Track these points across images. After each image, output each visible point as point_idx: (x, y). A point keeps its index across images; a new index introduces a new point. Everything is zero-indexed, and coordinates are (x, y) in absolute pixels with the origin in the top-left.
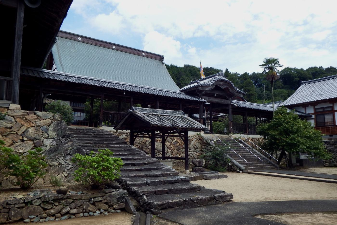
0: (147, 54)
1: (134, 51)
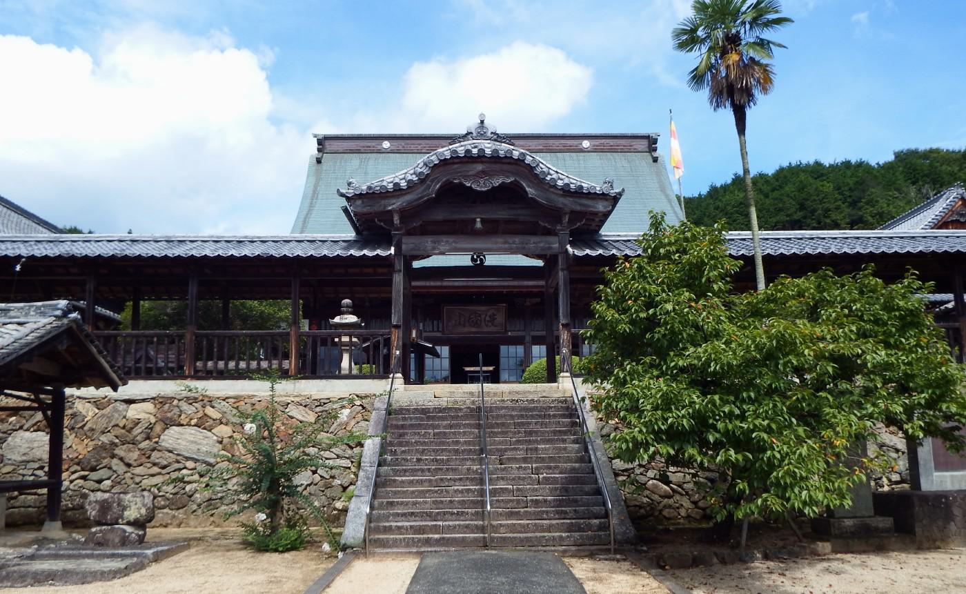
1: (551, 142)
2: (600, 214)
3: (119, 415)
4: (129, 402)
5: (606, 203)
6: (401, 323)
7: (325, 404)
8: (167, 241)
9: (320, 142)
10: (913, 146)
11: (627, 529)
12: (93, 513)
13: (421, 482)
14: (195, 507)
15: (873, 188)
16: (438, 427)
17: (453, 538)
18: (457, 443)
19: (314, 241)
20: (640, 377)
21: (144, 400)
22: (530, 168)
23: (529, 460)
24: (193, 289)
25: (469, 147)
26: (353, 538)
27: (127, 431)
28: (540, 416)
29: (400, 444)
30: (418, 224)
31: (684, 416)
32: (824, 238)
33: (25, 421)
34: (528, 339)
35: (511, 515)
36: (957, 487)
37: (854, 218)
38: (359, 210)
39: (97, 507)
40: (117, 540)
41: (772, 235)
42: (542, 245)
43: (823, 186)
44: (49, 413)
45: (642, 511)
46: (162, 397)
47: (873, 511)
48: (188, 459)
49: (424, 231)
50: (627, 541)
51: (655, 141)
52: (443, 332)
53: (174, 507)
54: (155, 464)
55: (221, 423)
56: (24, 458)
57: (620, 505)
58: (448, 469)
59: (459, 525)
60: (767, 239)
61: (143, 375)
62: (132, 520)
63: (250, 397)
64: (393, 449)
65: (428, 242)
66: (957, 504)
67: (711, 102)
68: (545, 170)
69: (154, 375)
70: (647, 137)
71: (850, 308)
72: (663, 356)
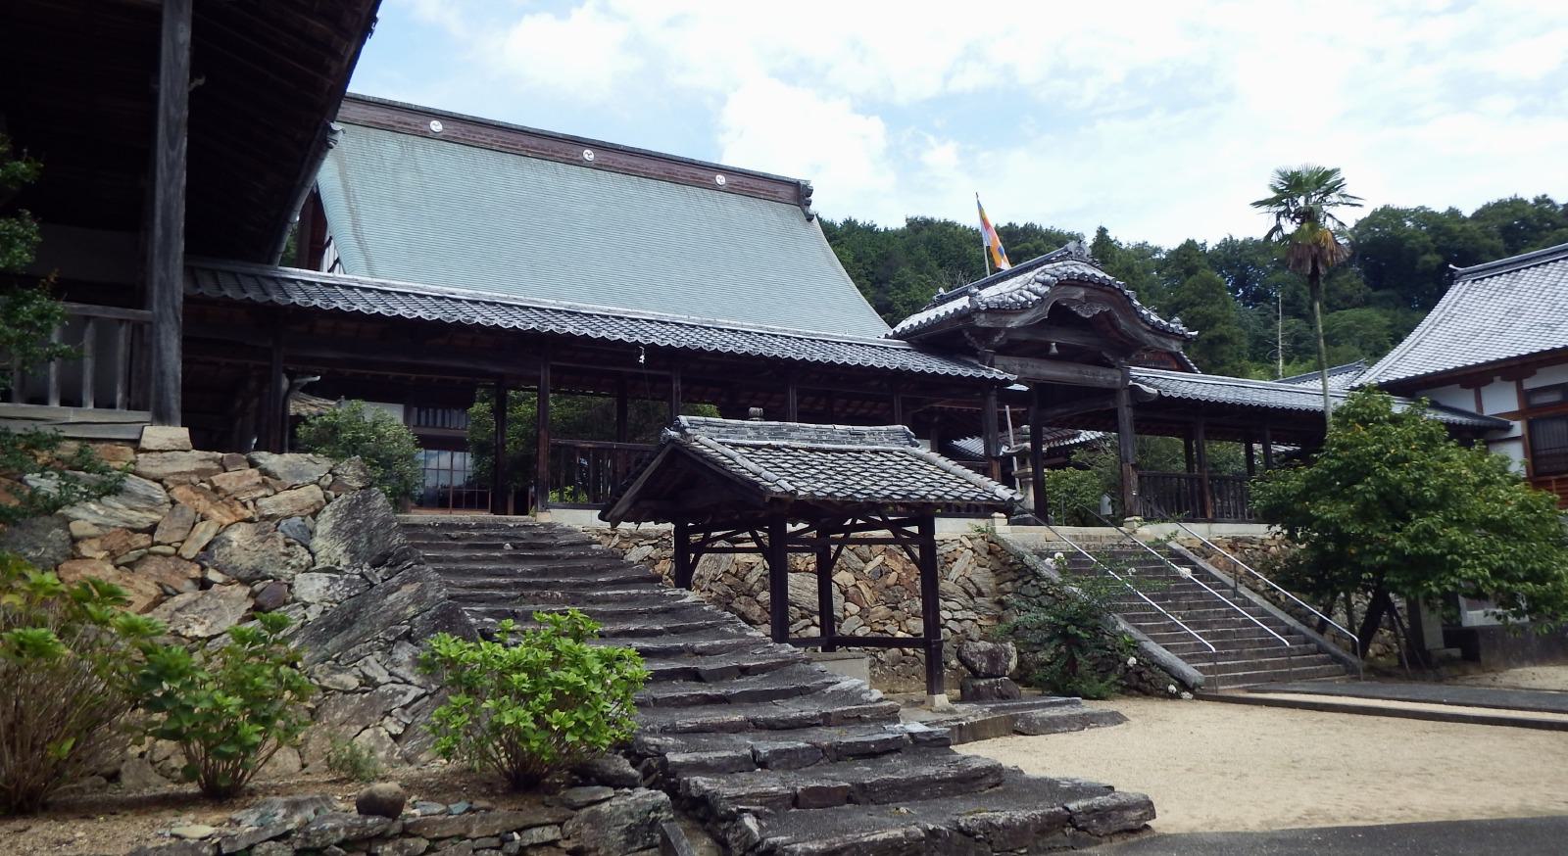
0: (735, 180)
1: (676, 168)
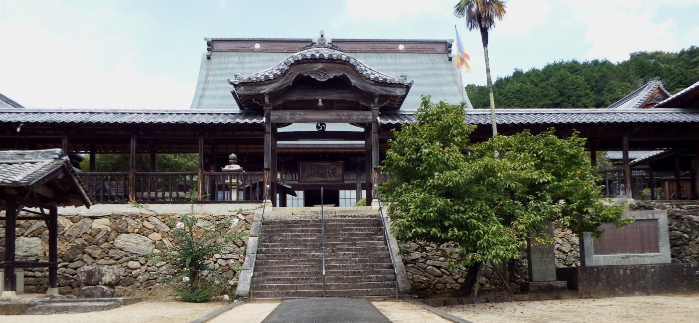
0: (409, 46)
1: (377, 45)
2: (399, 97)
3: (87, 227)
4: (94, 218)
5: (402, 90)
6: (270, 167)
7: (221, 219)
8: (113, 113)
9: (209, 44)
10: (643, 50)
11: (406, 285)
12: (83, 278)
13: (284, 263)
14: (138, 284)
15: (612, 80)
16: (294, 231)
17: (303, 292)
18: (306, 240)
19: (212, 114)
20: (411, 191)
21: (103, 217)
22: (353, 67)
23: (350, 250)
24: (133, 145)
25: (314, 53)
26: (243, 291)
27: (93, 237)
28: (359, 225)
29: (271, 241)
30: (281, 102)
31: (431, 212)
32: (543, 114)
33: (24, 231)
34: (359, 185)
35: (338, 279)
36: (607, 264)
37: (598, 102)
38: (242, 93)
39: (86, 275)
40: (99, 294)
41: (511, 111)
42: (361, 117)
43: (577, 78)
44: (49, 222)
45: (423, 285)
46: (115, 215)
47: (556, 278)
48: (133, 254)
49: (285, 107)
50: (406, 292)
51: (450, 46)
52: (299, 181)
53: (125, 285)
54: (111, 258)
55: (154, 231)
56: (25, 254)
57: (403, 273)
58: (300, 255)
59: (307, 285)
60: (507, 114)
61: (101, 201)
62: (107, 283)
63: (173, 215)
64: (266, 244)
65: (287, 115)
66: (603, 272)
67: (468, 25)
68: (363, 68)
69: (109, 201)
70: (445, 43)
71: (537, 153)
72: (424, 178)
